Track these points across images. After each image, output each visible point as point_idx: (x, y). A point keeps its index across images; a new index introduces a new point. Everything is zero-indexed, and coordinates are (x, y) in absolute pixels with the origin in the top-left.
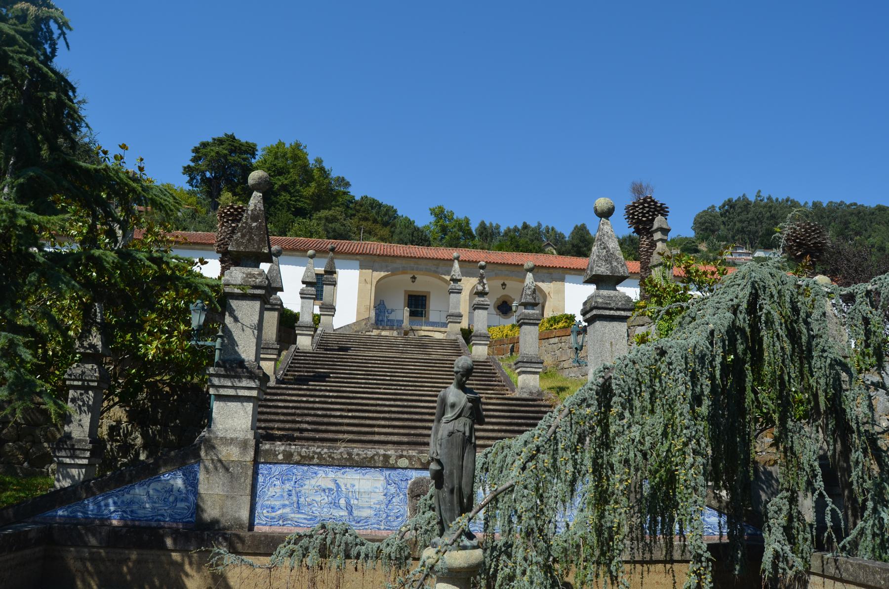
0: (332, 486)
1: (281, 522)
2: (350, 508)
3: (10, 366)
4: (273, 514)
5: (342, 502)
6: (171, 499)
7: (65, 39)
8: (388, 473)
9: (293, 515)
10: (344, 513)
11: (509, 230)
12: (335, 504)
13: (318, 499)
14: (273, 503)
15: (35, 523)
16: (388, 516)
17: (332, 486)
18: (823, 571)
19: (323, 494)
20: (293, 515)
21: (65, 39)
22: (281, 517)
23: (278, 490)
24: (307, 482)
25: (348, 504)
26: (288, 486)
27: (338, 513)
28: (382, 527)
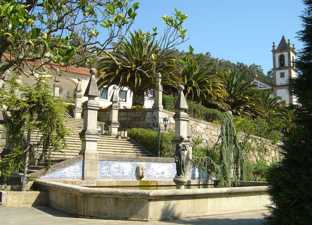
0: (119, 167)
1: (105, 177)
2: (123, 173)
3: (19, 19)
4: (103, 175)
5: (121, 172)
6: (76, 172)
7: (63, 30)
8: (132, 163)
9: (108, 175)
10: (122, 174)
11: (251, 65)
12: (119, 172)
13: (115, 170)
14: (103, 172)
15: (27, 156)
16: (132, 175)
17: (119, 167)
18: (140, 177)
19: (116, 169)
20: (108, 175)
21: (63, 30)
22: (105, 176)
23: (104, 168)
24: (112, 166)
25: (122, 171)
26: (107, 167)
27: (120, 174)
28: (131, 178)
